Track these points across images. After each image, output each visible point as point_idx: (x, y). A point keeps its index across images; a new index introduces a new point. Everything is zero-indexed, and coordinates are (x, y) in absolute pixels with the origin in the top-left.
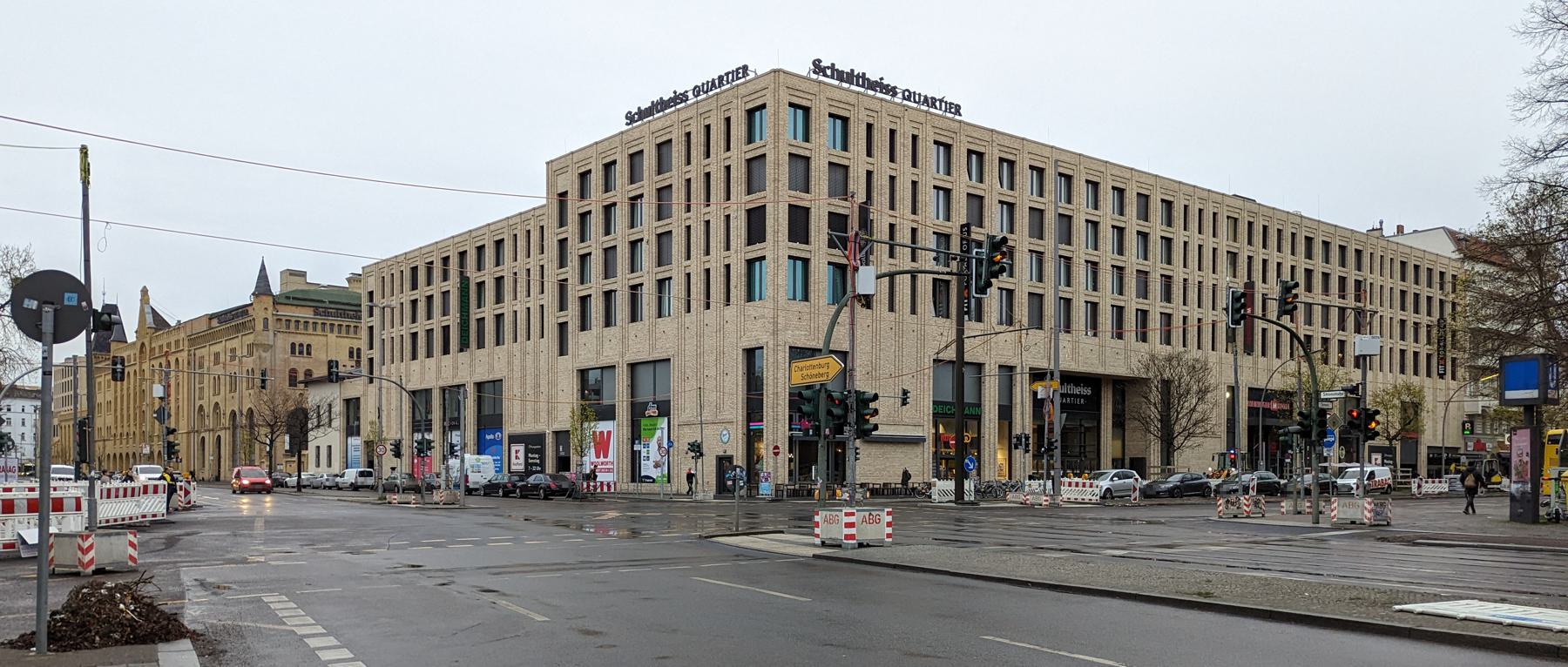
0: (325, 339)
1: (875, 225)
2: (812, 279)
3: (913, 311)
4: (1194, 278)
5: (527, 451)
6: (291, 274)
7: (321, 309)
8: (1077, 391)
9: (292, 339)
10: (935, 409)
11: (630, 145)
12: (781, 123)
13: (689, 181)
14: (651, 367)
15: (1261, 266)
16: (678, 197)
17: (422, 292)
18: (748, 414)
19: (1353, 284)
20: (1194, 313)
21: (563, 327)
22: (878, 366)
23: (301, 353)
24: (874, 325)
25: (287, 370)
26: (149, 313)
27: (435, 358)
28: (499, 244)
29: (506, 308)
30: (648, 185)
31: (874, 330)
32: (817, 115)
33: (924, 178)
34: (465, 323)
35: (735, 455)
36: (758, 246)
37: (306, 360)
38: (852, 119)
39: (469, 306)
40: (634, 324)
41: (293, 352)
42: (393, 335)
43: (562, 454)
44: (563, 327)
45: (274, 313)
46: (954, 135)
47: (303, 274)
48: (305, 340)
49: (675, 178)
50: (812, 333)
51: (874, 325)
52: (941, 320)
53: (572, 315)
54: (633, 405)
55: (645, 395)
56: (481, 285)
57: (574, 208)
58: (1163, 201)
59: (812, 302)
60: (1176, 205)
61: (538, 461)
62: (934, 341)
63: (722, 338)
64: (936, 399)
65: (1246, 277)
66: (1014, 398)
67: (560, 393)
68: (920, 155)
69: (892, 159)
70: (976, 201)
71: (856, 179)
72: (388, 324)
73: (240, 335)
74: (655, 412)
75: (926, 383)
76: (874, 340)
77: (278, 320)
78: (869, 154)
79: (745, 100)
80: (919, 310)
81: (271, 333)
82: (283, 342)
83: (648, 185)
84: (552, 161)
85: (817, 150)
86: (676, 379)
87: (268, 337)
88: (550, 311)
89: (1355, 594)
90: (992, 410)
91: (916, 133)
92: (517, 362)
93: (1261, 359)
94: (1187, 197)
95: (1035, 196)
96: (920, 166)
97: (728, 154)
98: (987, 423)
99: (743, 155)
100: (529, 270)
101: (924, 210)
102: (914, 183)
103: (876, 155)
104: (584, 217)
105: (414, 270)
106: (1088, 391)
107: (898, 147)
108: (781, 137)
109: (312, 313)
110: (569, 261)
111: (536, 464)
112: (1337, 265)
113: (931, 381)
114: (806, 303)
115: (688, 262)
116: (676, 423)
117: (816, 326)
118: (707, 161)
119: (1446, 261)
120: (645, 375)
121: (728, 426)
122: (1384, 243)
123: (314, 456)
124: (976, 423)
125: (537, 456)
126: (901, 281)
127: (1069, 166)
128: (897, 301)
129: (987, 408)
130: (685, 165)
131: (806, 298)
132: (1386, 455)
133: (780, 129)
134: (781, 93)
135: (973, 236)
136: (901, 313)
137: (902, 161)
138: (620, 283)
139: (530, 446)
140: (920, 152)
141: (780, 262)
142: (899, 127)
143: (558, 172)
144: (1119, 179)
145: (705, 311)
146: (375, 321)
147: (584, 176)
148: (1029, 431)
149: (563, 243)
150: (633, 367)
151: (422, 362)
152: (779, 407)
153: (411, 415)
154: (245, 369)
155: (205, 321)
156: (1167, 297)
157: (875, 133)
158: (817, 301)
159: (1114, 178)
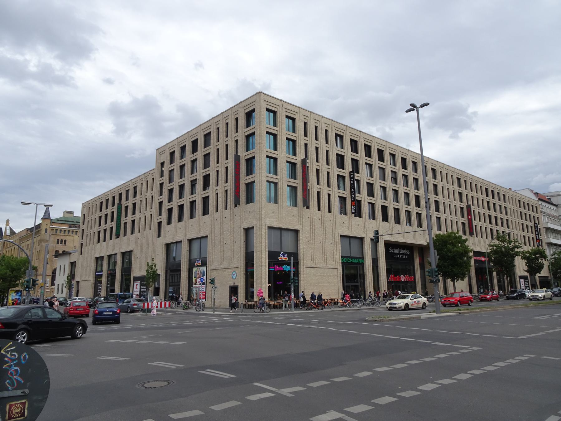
0: (73, 237)
1: (310, 169)
2: (279, 193)
3: (330, 211)
4: (447, 202)
5: (141, 285)
6: (67, 213)
7: (72, 225)
8: (404, 252)
9: (58, 238)
10: (342, 260)
11: (192, 137)
12: (262, 116)
13: (218, 149)
14: (199, 241)
15: (471, 199)
16: (213, 158)
17: (104, 211)
18: (247, 263)
19: (461, 225)
20: (449, 218)
21: (160, 223)
22: (314, 238)
23: (61, 243)
24: (311, 217)
25: (54, 251)
26: (8, 230)
27: (106, 242)
28: (135, 188)
29: (136, 217)
30: (199, 155)
31: (311, 220)
32: (280, 115)
33: (332, 149)
34: (118, 224)
35: (239, 285)
36: (251, 176)
37: (64, 247)
38: (297, 119)
39: (121, 217)
40: (191, 220)
41: (58, 243)
42: (91, 233)
43: (157, 286)
44: (160, 223)
45: (51, 226)
46: (344, 132)
47: (72, 213)
48: (64, 238)
49: (212, 149)
50: (280, 220)
51: (311, 217)
52: (343, 216)
53: (164, 218)
54: (190, 260)
55: (195, 255)
56: (127, 207)
57: (166, 169)
58: (404, 193)
59: (280, 204)
60: (437, 170)
61: (145, 290)
62: (340, 226)
63: (233, 224)
64: (342, 255)
65: (466, 203)
66: (378, 255)
67: (157, 256)
68: (329, 139)
69: (316, 139)
70: (355, 163)
71: (300, 147)
72: (89, 228)
73: (36, 236)
74: (200, 264)
75: (338, 247)
76: (311, 224)
77: (52, 229)
78: (306, 135)
79: (245, 108)
80: (332, 210)
81: (48, 235)
82: (53, 239)
83: (199, 155)
84: (159, 149)
85: (281, 131)
86: (210, 246)
87: (47, 237)
88: (154, 216)
89: (52, 228)
90: (369, 260)
91: (327, 129)
92: (139, 241)
93: (476, 238)
94: (441, 168)
95: (369, 177)
96: (329, 144)
97: (237, 134)
98: (367, 267)
99: (244, 133)
100: (147, 198)
101: (332, 164)
102: (327, 151)
103: (309, 136)
104: (171, 171)
105: (102, 203)
106: (408, 252)
107: (319, 134)
108: (262, 123)
109: (68, 226)
110: (164, 192)
111: (144, 292)
112: (460, 217)
113: (340, 245)
114: (276, 205)
115: (217, 188)
116: (210, 269)
117: (282, 216)
118: (227, 139)
119: (533, 201)
120: (196, 245)
121: (236, 270)
122: (512, 193)
123: (57, 289)
124: (361, 267)
125: (145, 287)
126: (323, 196)
127: (394, 150)
128: (322, 206)
129: (367, 259)
130: (217, 142)
131: (276, 201)
132: (525, 280)
133: (262, 119)
134: (262, 103)
135: (356, 178)
136: (324, 212)
137: (321, 140)
138: (185, 201)
139: (142, 283)
140: (329, 137)
141: (262, 183)
142: (319, 125)
143: (161, 154)
144: (414, 158)
145: (225, 211)
146: (85, 227)
147: (172, 154)
148: (146, 308)
149: (162, 184)
150: (190, 241)
151: (101, 244)
152: (263, 259)
153: (95, 269)
154: (37, 251)
155: (26, 231)
156: (437, 210)
157: (308, 126)
158: (282, 203)
159: (412, 157)
